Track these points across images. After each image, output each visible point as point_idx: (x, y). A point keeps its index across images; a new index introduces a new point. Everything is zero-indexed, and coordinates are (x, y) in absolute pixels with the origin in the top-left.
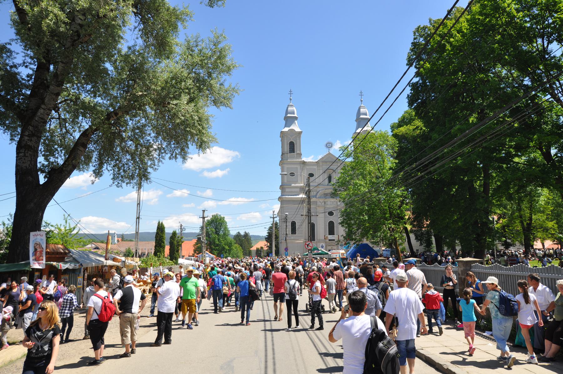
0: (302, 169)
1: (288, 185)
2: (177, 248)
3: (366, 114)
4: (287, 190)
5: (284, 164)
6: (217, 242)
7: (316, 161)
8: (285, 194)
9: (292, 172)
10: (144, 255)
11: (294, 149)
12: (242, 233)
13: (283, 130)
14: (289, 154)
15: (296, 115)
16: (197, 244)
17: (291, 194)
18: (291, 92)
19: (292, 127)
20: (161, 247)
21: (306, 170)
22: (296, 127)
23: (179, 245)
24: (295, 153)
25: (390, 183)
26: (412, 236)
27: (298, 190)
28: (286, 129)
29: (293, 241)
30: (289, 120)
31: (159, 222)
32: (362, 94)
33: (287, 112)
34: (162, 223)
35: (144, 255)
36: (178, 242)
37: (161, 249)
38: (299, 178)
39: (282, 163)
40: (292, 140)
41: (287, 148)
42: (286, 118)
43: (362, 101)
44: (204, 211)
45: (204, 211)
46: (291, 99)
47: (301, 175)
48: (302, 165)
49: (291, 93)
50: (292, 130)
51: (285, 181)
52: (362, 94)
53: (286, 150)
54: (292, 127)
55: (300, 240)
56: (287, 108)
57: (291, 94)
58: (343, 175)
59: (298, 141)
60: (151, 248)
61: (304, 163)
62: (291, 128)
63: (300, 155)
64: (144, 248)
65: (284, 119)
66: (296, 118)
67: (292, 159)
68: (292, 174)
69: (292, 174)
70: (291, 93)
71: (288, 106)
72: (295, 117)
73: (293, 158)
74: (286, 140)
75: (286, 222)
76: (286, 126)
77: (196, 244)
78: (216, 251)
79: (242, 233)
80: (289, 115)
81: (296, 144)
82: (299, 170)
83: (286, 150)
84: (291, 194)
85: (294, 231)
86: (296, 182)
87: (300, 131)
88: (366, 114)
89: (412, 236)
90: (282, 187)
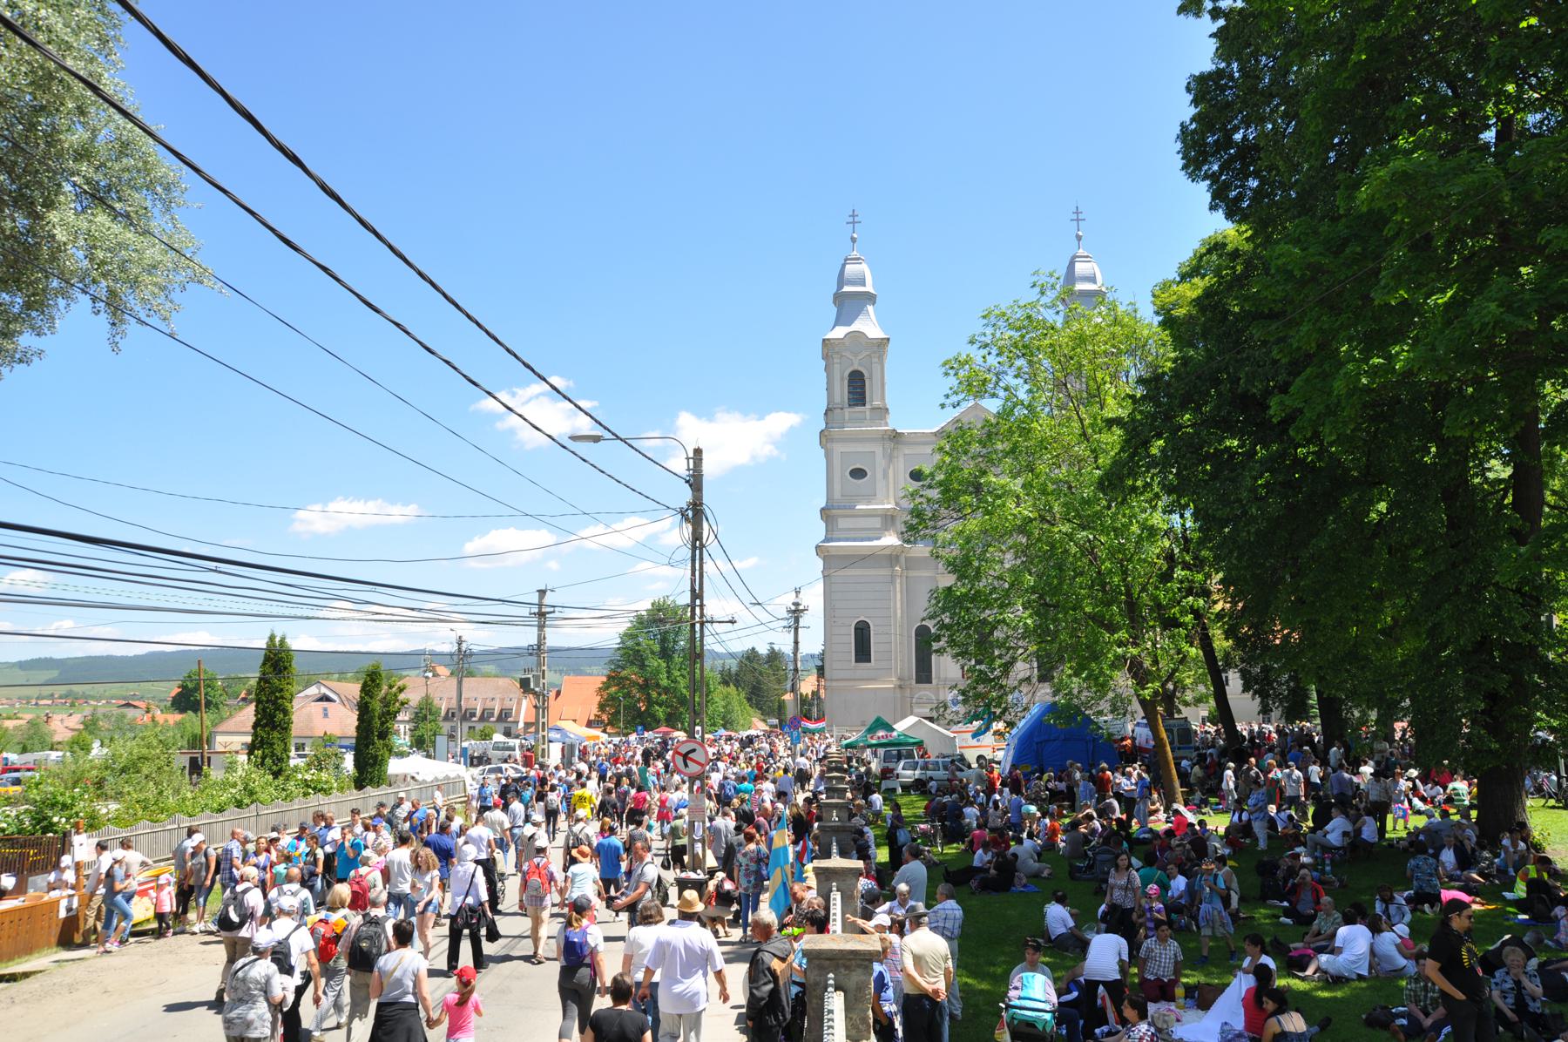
0: (890, 458)
1: (845, 508)
2: (383, 723)
3: (1093, 279)
4: (843, 523)
5: (832, 440)
6: (664, 682)
7: (935, 430)
8: (836, 535)
9: (858, 466)
10: (473, 715)
11: (863, 393)
12: (763, 650)
13: (830, 336)
14: (847, 411)
15: (869, 288)
16: (608, 688)
17: (852, 535)
18: (853, 216)
19: (856, 326)
20: (274, 728)
21: (901, 460)
22: (869, 325)
23: (389, 713)
24: (868, 406)
25: (1115, 482)
26: (1234, 681)
27: (877, 523)
28: (839, 332)
29: (851, 683)
30: (849, 304)
31: (272, 638)
32: (1081, 217)
33: (842, 280)
34: (283, 640)
35: (473, 715)
36: (386, 702)
37: (276, 734)
38: (880, 484)
39: (825, 438)
40: (856, 367)
41: (842, 391)
42: (840, 299)
43: (1079, 238)
44: (542, 593)
45: (542, 593)
46: (854, 240)
47: (885, 476)
48: (891, 445)
49: (854, 220)
50: (858, 335)
51: (837, 495)
52: (1081, 217)
53: (837, 399)
54: (857, 326)
55: (885, 682)
56: (844, 266)
57: (854, 223)
58: (948, 459)
59: (876, 368)
60: (491, 696)
61: (895, 437)
62: (853, 328)
63: (883, 411)
64: (475, 695)
65: (835, 303)
66: (870, 298)
67: (857, 424)
68: (858, 473)
69: (858, 473)
70: (854, 220)
71: (846, 259)
72: (868, 293)
73: (862, 420)
74: (837, 367)
75: (796, 629)
76: (838, 322)
77: (606, 686)
78: (660, 706)
79: (763, 650)
80: (847, 289)
81: (871, 378)
82: (880, 462)
83: (837, 399)
84: (852, 535)
85: (863, 651)
86: (870, 497)
87: (883, 336)
88: (1093, 279)
89: (1234, 681)
90: (826, 513)
